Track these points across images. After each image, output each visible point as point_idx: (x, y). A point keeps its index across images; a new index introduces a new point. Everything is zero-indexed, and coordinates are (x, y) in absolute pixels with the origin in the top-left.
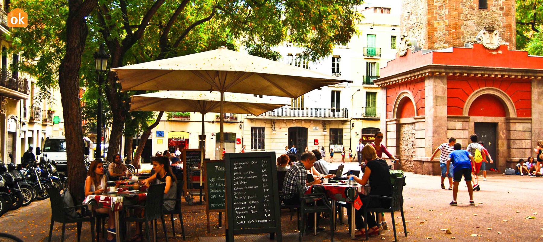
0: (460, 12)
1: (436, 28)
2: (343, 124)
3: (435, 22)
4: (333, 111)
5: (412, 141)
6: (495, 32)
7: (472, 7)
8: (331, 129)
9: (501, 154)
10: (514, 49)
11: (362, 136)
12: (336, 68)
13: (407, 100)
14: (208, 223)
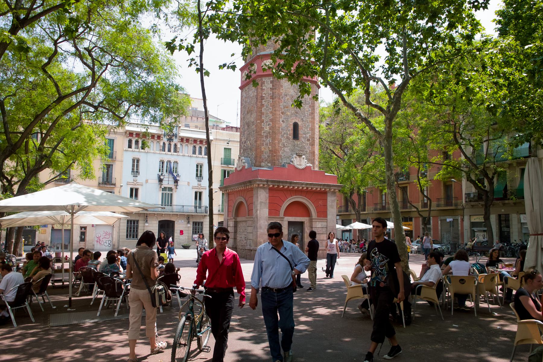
1: (263, 152)
3: (262, 147)
4: (196, 207)
5: (245, 235)
7: (288, 138)
12: (199, 173)
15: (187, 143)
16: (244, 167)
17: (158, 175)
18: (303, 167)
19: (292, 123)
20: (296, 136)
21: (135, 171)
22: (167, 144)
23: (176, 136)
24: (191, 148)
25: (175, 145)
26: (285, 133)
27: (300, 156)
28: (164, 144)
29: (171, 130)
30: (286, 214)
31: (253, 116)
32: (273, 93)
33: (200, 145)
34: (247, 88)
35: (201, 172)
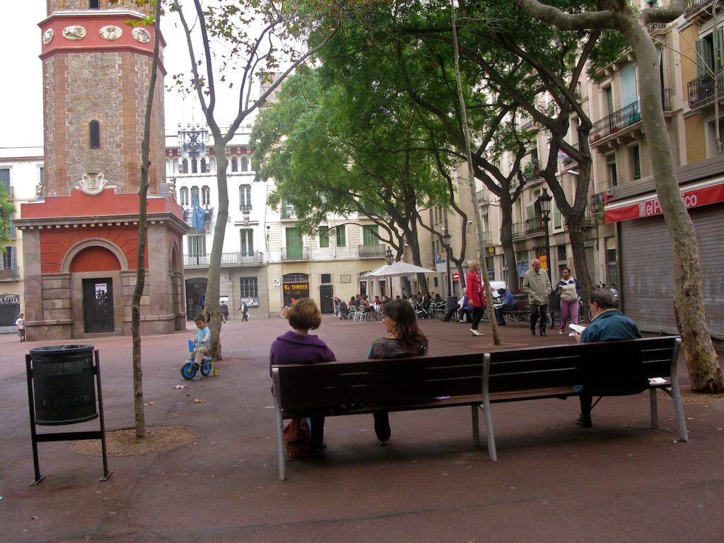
0: (66, 155)
2: (257, 271)
8: (241, 279)
20: (95, 141)
25: (203, 161)
27: (93, 174)
28: (185, 161)
29: (194, 139)
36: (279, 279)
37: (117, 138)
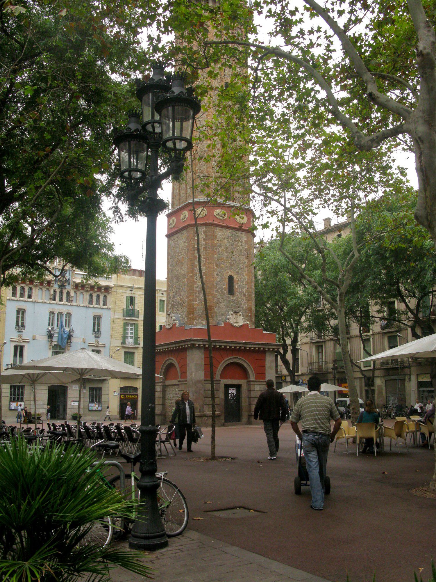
2: (102, 383)
6: (240, 313)
7: (223, 293)
8: (90, 388)
9: (244, 409)
10: (253, 327)
11: (121, 395)
12: (96, 327)
13: (171, 365)
14: (213, 427)
15: (82, 291)
16: (174, 325)
17: (48, 329)
18: (240, 324)
19: (226, 277)
20: (231, 290)
21: (20, 326)
22: (58, 291)
23: (68, 282)
24: (87, 296)
25: (68, 293)
26: (219, 288)
27: (236, 313)
30: (222, 376)
31: (183, 268)
32: (206, 244)
33: (98, 293)
34: (175, 236)
35: (99, 325)
36: (118, 390)
37: (244, 290)
